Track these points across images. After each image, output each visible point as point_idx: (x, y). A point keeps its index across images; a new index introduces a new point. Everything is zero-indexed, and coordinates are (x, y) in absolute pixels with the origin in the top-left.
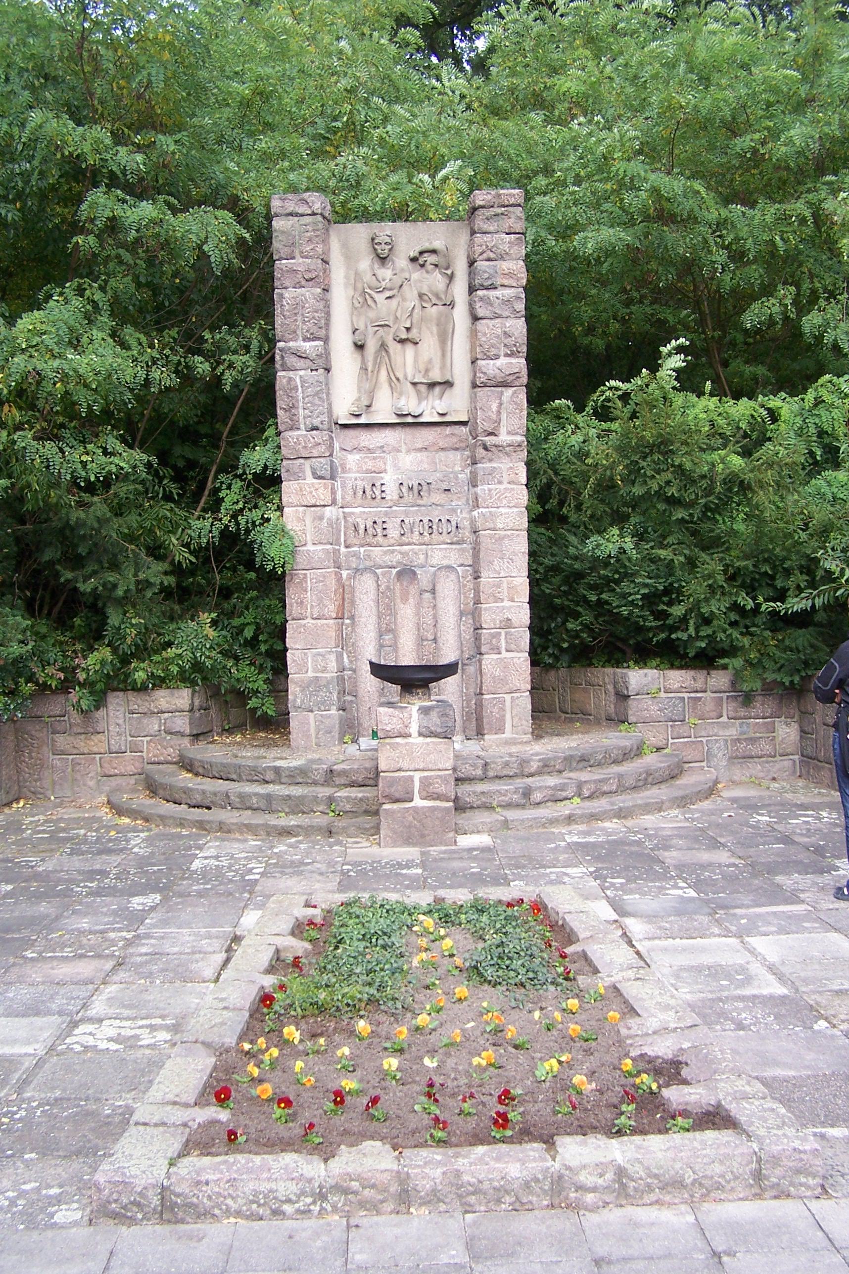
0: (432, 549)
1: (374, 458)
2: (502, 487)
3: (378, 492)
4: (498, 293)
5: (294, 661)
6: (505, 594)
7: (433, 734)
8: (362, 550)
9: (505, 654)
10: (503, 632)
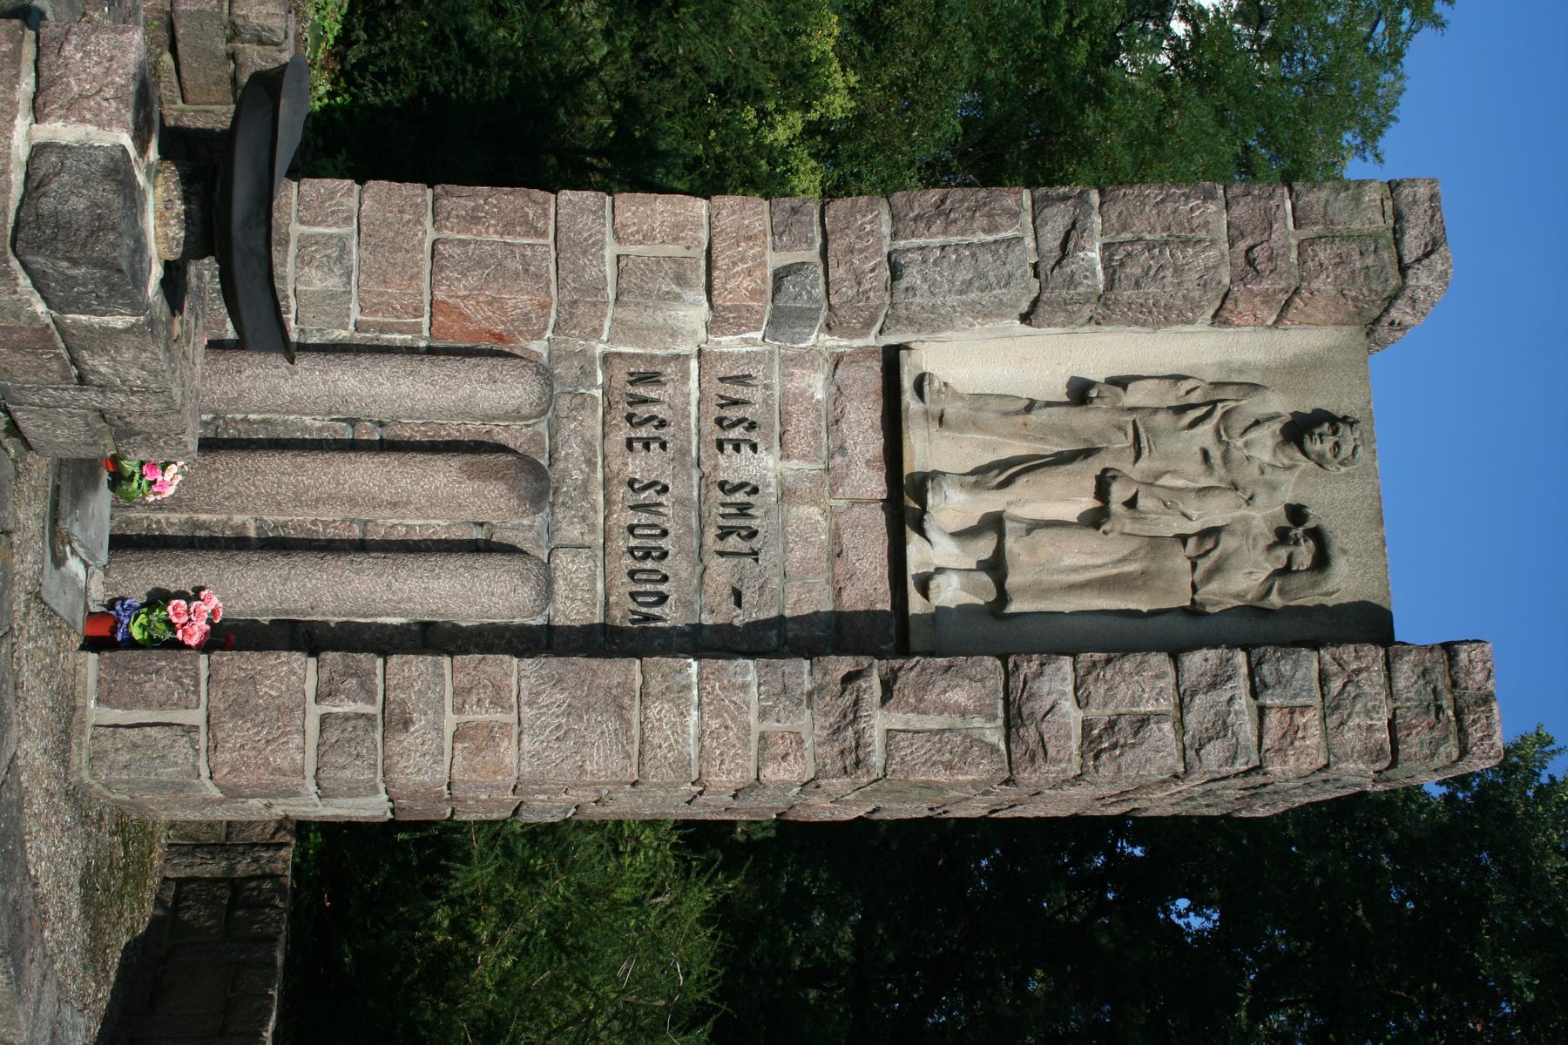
0: (594, 557)
1: (815, 433)
2: (752, 719)
3: (735, 434)
4: (1243, 702)
5: (332, 194)
6: (478, 715)
7: (34, 186)
8: (598, 393)
9: (314, 712)
10: (376, 709)
